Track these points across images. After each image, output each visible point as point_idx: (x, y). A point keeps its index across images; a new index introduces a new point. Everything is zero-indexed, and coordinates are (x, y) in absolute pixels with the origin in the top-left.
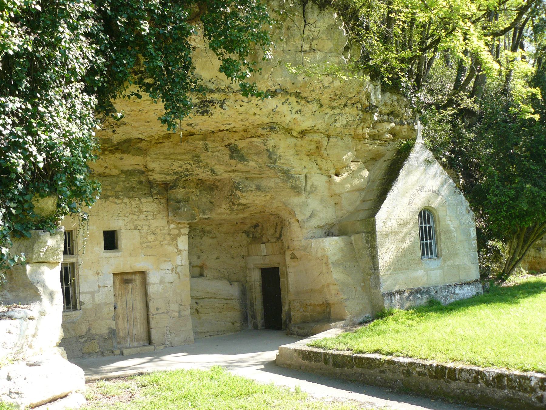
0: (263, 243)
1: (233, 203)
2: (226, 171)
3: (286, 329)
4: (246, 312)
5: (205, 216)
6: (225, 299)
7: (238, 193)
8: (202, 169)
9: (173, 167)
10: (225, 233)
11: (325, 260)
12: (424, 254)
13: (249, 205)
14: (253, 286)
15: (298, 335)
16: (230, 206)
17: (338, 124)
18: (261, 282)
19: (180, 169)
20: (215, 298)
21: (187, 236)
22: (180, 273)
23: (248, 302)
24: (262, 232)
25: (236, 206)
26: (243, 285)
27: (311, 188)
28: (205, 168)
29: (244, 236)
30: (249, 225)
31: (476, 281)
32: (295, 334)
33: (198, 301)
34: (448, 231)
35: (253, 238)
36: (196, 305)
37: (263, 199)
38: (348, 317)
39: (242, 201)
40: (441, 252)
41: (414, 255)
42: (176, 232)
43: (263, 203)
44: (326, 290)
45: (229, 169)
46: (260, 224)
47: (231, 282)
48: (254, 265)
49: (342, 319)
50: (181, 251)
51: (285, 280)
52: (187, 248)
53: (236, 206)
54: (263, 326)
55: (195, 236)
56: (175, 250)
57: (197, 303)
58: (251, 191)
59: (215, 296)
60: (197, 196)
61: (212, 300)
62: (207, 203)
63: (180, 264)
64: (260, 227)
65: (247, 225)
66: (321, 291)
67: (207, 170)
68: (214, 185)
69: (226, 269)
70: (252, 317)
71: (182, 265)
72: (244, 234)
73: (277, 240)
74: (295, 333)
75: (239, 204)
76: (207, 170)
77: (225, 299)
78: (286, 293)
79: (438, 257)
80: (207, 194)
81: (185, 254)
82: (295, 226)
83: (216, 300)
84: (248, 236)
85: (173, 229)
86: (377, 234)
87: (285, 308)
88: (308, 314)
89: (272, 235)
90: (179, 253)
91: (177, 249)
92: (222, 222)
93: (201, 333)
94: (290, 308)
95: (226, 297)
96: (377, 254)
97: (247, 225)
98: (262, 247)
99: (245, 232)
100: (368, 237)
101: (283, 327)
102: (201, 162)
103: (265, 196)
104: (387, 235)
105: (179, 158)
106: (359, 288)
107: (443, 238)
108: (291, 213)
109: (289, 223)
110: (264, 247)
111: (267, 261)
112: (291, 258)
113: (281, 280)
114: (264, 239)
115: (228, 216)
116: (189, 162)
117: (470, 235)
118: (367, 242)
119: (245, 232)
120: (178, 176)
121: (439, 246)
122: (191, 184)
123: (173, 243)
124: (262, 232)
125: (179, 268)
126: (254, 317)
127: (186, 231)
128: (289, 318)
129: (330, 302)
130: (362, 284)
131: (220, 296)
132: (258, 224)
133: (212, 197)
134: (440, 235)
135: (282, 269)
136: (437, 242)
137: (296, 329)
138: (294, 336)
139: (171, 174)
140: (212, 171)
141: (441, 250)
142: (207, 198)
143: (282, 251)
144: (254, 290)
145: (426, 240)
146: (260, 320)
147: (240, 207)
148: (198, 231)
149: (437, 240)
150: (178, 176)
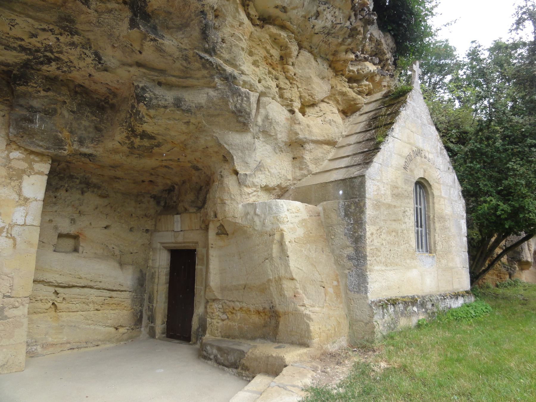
0: (177, 214)
1: (133, 131)
2: (124, 64)
3: (195, 343)
4: (141, 312)
5: (84, 150)
6: (109, 290)
7: (142, 108)
8: (78, 49)
9: (16, 32)
10: (123, 194)
11: (277, 237)
12: (418, 247)
13: (160, 139)
14: (157, 274)
15: (216, 361)
16: (128, 138)
17: (319, 24)
18: (169, 269)
19: (33, 40)
20: (91, 287)
21: (46, 178)
22: (18, 239)
23: (146, 296)
24: (178, 199)
25: (138, 139)
26: (141, 271)
27: (263, 121)
28: (83, 47)
29: (153, 203)
30: (161, 188)
31: (467, 292)
32: (211, 359)
33: (59, 290)
34: (442, 218)
35: (164, 207)
36: (54, 297)
37: (184, 128)
38: (316, 341)
39: (148, 128)
40: (435, 247)
41: (407, 245)
42: (24, 165)
43: (183, 138)
44: (273, 289)
45: (129, 61)
46: (176, 187)
47: (122, 264)
48: (162, 243)
49: (304, 345)
50: (26, 200)
51: (204, 268)
52: (41, 195)
53: (138, 139)
54: (163, 333)
55: (71, 188)
56: (15, 196)
57: (56, 293)
58: (165, 107)
59: (92, 284)
60: (73, 112)
61: (86, 290)
62: (91, 130)
63: (21, 221)
64: (176, 192)
65: (157, 186)
66: (263, 289)
67: (87, 52)
68: (107, 103)
69: (118, 246)
70: (149, 319)
71: (25, 225)
72: (153, 199)
73: (197, 210)
74: (212, 357)
75: (144, 135)
76: (87, 52)
77: (109, 290)
78: (203, 288)
79: (430, 253)
80: (93, 113)
81: (37, 207)
82: (230, 182)
83: (92, 291)
84: (158, 203)
85: (19, 159)
86: (367, 201)
87: (199, 310)
88: (235, 325)
89: (193, 202)
90: (21, 202)
91: (20, 195)
92: (119, 173)
93: (52, 345)
94: (206, 312)
95: (110, 287)
96: (365, 234)
97: (157, 186)
98: (175, 219)
99: (154, 197)
100: (349, 206)
101: (193, 339)
102: (77, 33)
103: (188, 123)
104: (408, 197)
105: (31, 13)
106: (331, 290)
107: (437, 225)
108: (227, 158)
109: (222, 176)
110: (179, 219)
111: (180, 239)
112: (218, 234)
113: (198, 267)
114: (180, 207)
115: (124, 158)
116: (51, 27)
117: (461, 229)
118: (346, 215)
119: (154, 197)
120: (31, 57)
121: (432, 237)
122: (62, 88)
123: (13, 184)
124: (178, 199)
125: (16, 228)
126: (152, 319)
127: (45, 167)
128: (203, 327)
129: (280, 309)
130: (335, 283)
131: (101, 285)
132: (173, 187)
133: (101, 121)
134: (434, 223)
135: (200, 251)
136: (430, 231)
137: (215, 351)
138: (209, 362)
139: (14, 49)
140: (98, 57)
141: (435, 243)
142: (92, 121)
143: (203, 226)
144: (156, 280)
145: (421, 227)
146: (160, 325)
147: (146, 143)
148: (78, 181)
149: (429, 228)
150: (31, 57)
